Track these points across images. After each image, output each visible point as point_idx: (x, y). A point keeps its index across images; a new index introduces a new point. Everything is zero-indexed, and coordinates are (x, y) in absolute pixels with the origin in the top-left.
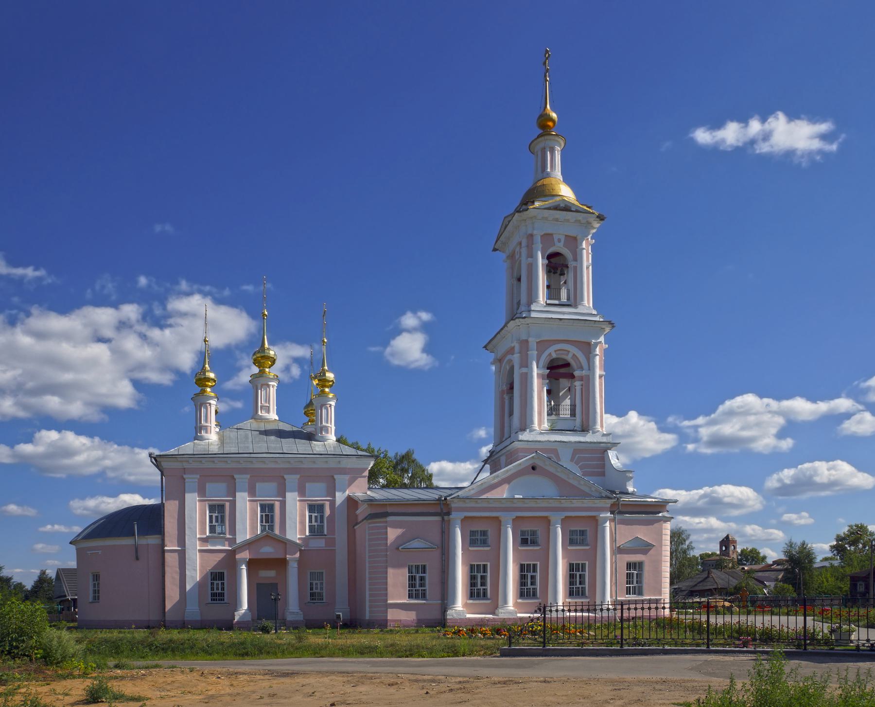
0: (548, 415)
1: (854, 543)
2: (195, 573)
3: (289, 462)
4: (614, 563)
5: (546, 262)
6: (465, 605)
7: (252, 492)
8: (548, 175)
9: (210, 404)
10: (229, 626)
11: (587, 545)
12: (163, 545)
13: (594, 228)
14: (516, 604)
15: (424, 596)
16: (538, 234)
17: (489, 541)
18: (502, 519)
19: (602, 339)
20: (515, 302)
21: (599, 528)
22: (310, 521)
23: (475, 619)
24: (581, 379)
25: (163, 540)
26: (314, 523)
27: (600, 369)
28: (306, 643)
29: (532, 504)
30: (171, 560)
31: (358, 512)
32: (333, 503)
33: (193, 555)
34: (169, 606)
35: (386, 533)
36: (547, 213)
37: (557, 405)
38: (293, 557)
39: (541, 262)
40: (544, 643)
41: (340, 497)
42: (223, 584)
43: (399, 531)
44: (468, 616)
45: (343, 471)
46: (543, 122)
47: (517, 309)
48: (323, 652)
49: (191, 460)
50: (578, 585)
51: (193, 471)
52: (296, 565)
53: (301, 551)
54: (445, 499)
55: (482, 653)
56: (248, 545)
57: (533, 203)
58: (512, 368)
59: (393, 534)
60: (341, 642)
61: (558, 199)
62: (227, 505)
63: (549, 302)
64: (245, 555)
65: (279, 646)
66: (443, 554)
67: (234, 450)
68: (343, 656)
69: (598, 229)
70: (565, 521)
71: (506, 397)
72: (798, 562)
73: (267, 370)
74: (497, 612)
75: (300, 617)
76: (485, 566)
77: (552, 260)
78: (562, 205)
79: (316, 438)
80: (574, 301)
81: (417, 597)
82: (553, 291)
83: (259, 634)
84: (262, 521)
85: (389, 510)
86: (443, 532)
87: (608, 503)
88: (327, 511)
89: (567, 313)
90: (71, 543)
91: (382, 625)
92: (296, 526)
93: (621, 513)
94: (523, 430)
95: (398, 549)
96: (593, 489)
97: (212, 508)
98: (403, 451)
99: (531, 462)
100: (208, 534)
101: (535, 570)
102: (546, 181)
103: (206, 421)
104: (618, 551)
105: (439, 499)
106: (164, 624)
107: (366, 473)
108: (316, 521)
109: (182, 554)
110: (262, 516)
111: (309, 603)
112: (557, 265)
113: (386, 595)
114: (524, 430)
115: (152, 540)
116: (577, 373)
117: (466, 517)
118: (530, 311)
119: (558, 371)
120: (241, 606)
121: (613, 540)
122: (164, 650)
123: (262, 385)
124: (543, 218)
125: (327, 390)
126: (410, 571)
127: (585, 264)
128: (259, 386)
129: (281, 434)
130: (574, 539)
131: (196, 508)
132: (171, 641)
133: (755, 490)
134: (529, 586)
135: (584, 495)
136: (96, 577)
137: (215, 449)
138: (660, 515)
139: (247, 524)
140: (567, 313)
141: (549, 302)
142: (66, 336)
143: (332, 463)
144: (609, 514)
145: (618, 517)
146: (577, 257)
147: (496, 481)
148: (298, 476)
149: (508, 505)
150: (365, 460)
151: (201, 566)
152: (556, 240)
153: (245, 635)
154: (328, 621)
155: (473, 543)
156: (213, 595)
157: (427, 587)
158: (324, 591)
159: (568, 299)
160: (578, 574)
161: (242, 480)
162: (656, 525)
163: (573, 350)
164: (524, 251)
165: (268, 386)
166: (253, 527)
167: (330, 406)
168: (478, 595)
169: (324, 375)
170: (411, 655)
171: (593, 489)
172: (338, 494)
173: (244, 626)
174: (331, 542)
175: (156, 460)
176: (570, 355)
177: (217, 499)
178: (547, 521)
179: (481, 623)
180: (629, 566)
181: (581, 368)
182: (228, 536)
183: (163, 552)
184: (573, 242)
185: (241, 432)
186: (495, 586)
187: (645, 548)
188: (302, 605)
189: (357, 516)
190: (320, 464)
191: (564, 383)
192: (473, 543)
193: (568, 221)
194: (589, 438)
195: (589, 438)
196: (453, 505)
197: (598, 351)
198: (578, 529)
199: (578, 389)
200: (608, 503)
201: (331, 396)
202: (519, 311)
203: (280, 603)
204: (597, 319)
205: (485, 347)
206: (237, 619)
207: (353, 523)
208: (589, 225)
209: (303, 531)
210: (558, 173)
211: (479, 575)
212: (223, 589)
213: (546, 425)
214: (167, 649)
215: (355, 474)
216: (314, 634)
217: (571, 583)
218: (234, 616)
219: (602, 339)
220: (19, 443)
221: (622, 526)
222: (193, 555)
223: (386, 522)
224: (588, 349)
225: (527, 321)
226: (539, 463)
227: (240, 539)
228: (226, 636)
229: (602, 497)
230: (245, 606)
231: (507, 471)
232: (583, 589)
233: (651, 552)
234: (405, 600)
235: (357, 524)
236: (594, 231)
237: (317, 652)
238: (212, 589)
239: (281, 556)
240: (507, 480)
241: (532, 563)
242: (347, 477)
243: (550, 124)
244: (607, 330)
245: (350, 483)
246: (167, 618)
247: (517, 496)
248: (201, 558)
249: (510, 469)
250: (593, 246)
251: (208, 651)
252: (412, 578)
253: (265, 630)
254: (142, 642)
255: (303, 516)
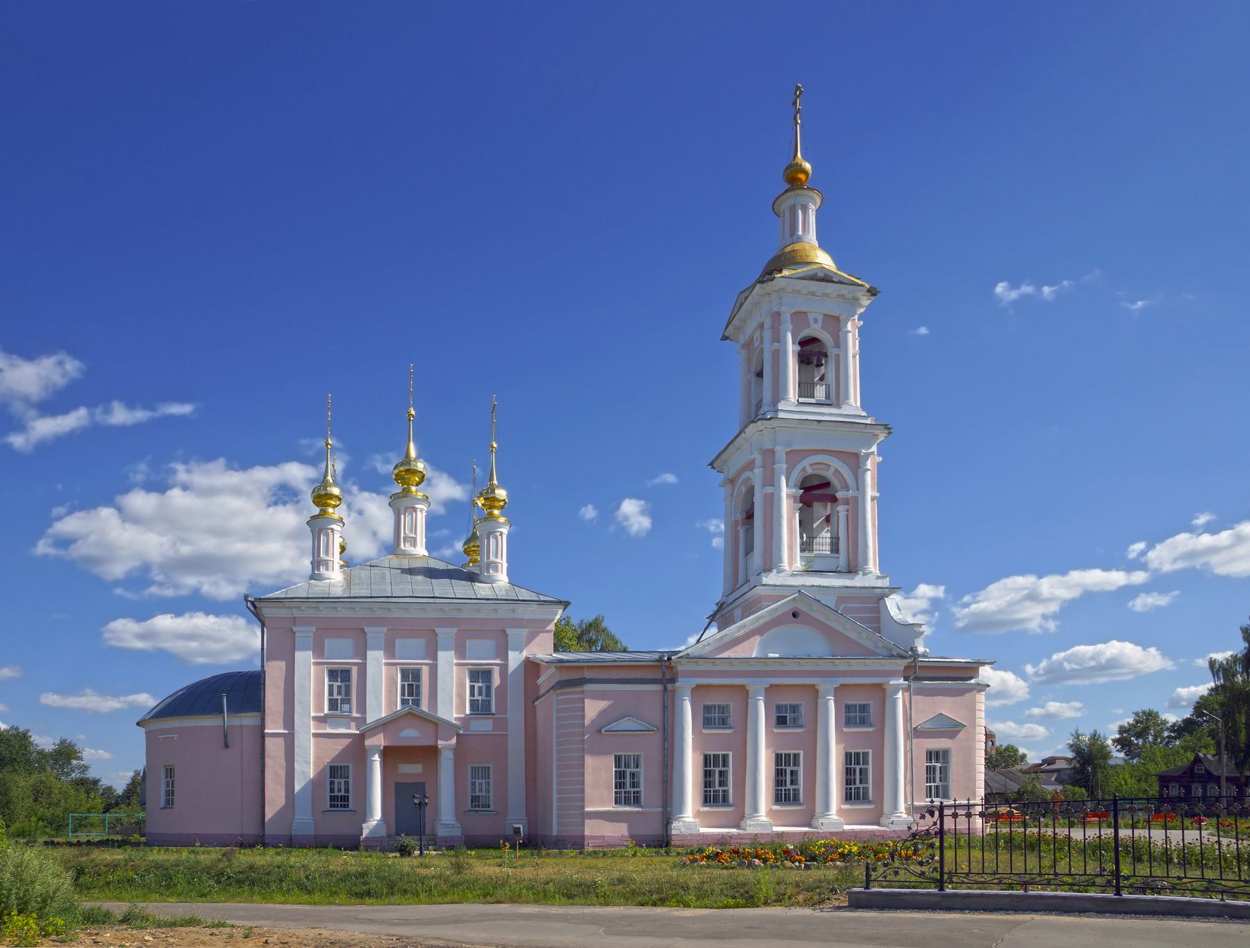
0: (802, 550)
1: (1141, 734)
2: (308, 766)
3: (442, 610)
4: (909, 751)
5: (798, 348)
6: (698, 814)
7: (390, 651)
8: (799, 240)
9: (333, 530)
10: (352, 844)
11: (871, 725)
12: (263, 727)
13: (862, 306)
14: (770, 813)
15: (637, 801)
16: (787, 312)
17: (731, 721)
18: (750, 689)
19: (874, 449)
20: (753, 402)
21: (888, 700)
22: (472, 694)
23: (712, 835)
24: (847, 502)
25: (263, 719)
26: (477, 697)
27: (873, 488)
28: (468, 875)
29: (792, 666)
30: (274, 748)
31: (540, 681)
32: (504, 668)
33: (304, 740)
34: (269, 813)
35: (583, 709)
36: (800, 285)
37: (811, 538)
38: (447, 744)
39: (791, 349)
40: (940, 884)
41: (515, 659)
42: (347, 783)
43: (603, 704)
44: (703, 830)
45: (520, 623)
46: (793, 179)
47: (756, 412)
48: (500, 892)
49: (303, 606)
50: (858, 785)
51: (308, 621)
52: (451, 755)
53: (458, 735)
54: (669, 659)
55: (801, 898)
56: (383, 726)
57: (780, 271)
58: (751, 491)
59: (593, 709)
60: (528, 873)
61: (815, 267)
62: (355, 670)
63: (801, 400)
64: (379, 741)
65: (423, 880)
66: (665, 739)
67: (364, 592)
68: (536, 902)
69: (868, 307)
70: (839, 691)
71: (741, 530)
72: (1088, 758)
73: (413, 488)
74: (742, 823)
75: (457, 832)
76: (725, 757)
77: (807, 348)
78: (821, 274)
79: (481, 578)
80: (835, 398)
81: (627, 802)
82: (806, 389)
83: (393, 858)
84: (403, 694)
85: (588, 674)
86: (665, 707)
87: (902, 663)
88: (496, 680)
89: (828, 414)
90: (138, 724)
91: (578, 843)
92: (452, 700)
93: (917, 679)
94: (768, 570)
95: (600, 731)
96: (880, 644)
97: (333, 674)
98: (589, 618)
99: (790, 607)
100: (326, 711)
101: (796, 763)
102: (797, 246)
103: (327, 553)
104: (915, 733)
105: (660, 660)
106: (260, 841)
107: (552, 627)
108: (480, 694)
109: (289, 740)
110: (403, 687)
111: (470, 808)
112: (812, 354)
113: (583, 800)
114: (770, 570)
115: (247, 720)
116: (839, 495)
117: (698, 686)
118: (777, 411)
119: (815, 492)
120: (372, 816)
121: (908, 719)
122: (240, 883)
123: (406, 508)
124: (794, 291)
125: (496, 512)
126: (618, 765)
127: (850, 352)
128: (402, 510)
129: (431, 573)
130: (854, 716)
131: (310, 674)
132: (251, 867)
133: (1015, 673)
134: (789, 786)
135: (869, 654)
136: (170, 772)
137: (338, 591)
138: (973, 681)
139: (381, 695)
140: (828, 414)
141: (801, 400)
142: (237, 491)
143: (504, 612)
144: (901, 681)
145: (914, 685)
146: (840, 342)
147: (742, 632)
148: (455, 630)
149: (757, 669)
150: (548, 609)
151: (317, 757)
152: (811, 323)
153: (372, 861)
154: (507, 839)
155: (708, 723)
156: (333, 798)
157: (642, 788)
158: (491, 794)
159: (828, 396)
160: (858, 768)
161: (375, 634)
162: (967, 696)
163: (835, 463)
164: (767, 334)
165: (415, 510)
166: (391, 702)
167: (501, 534)
168: (716, 800)
169: (493, 491)
170: (662, 902)
171: (880, 644)
172: (511, 654)
173: (374, 844)
174: (501, 724)
175: (255, 606)
176: (832, 470)
177: (340, 661)
178: (813, 691)
179: (722, 841)
180: (932, 755)
181: (847, 488)
182: (355, 715)
183: (263, 736)
184: (835, 323)
185: (375, 570)
186: (740, 785)
187: (952, 729)
188: (460, 813)
189: (538, 687)
190: (486, 613)
191: (821, 510)
192: (708, 723)
193: (828, 295)
194: (858, 581)
195: (858, 581)
196: (680, 668)
197: (869, 464)
198: (858, 702)
199: (842, 515)
200: (902, 663)
201: (502, 520)
202: (761, 412)
203: (428, 810)
204: (868, 421)
205: (711, 464)
206: (365, 833)
207: (532, 696)
208: (855, 301)
209: (461, 707)
210: (812, 237)
211: (717, 770)
212: (347, 791)
213: (799, 565)
214: (243, 882)
215: (536, 627)
216: (479, 857)
217: (848, 782)
218: (361, 829)
219: (874, 449)
220: (115, 619)
221: (919, 698)
222: (304, 740)
223: (583, 692)
224: (855, 461)
225: (774, 423)
226: (802, 607)
227: (371, 718)
228: (345, 861)
229: (892, 656)
230: (378, 814)
231: (758, 618)
232: (796, 792)
233: (961, 735)
234: (611, 807)
235: (538, 698)
236: (862, 310)
237: (489, 892)
238: (332, 790)
239: (430, 743)
240: (760, 631)
241: (792, 752)
242: (524, 632)
243: (802, 176)
244: (882, 437)
245: (530, 640)
246: (267, 832)
247: (771, 655)
248: (317, 746)
249: (763, 617)
250: (860, 329)
251: (306, 887)
252: (620, 775)
253: (404, 851)
254: (207, 870)
255: (461, 686)
